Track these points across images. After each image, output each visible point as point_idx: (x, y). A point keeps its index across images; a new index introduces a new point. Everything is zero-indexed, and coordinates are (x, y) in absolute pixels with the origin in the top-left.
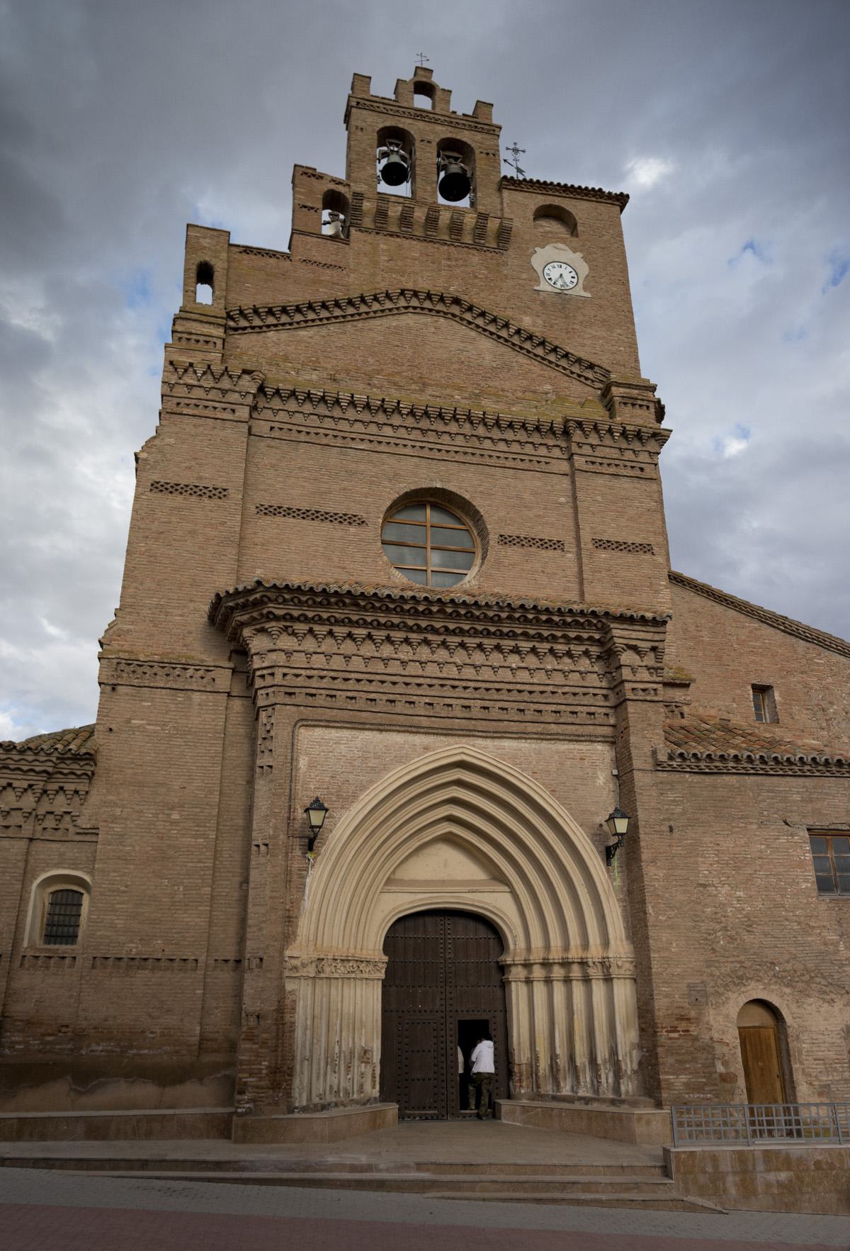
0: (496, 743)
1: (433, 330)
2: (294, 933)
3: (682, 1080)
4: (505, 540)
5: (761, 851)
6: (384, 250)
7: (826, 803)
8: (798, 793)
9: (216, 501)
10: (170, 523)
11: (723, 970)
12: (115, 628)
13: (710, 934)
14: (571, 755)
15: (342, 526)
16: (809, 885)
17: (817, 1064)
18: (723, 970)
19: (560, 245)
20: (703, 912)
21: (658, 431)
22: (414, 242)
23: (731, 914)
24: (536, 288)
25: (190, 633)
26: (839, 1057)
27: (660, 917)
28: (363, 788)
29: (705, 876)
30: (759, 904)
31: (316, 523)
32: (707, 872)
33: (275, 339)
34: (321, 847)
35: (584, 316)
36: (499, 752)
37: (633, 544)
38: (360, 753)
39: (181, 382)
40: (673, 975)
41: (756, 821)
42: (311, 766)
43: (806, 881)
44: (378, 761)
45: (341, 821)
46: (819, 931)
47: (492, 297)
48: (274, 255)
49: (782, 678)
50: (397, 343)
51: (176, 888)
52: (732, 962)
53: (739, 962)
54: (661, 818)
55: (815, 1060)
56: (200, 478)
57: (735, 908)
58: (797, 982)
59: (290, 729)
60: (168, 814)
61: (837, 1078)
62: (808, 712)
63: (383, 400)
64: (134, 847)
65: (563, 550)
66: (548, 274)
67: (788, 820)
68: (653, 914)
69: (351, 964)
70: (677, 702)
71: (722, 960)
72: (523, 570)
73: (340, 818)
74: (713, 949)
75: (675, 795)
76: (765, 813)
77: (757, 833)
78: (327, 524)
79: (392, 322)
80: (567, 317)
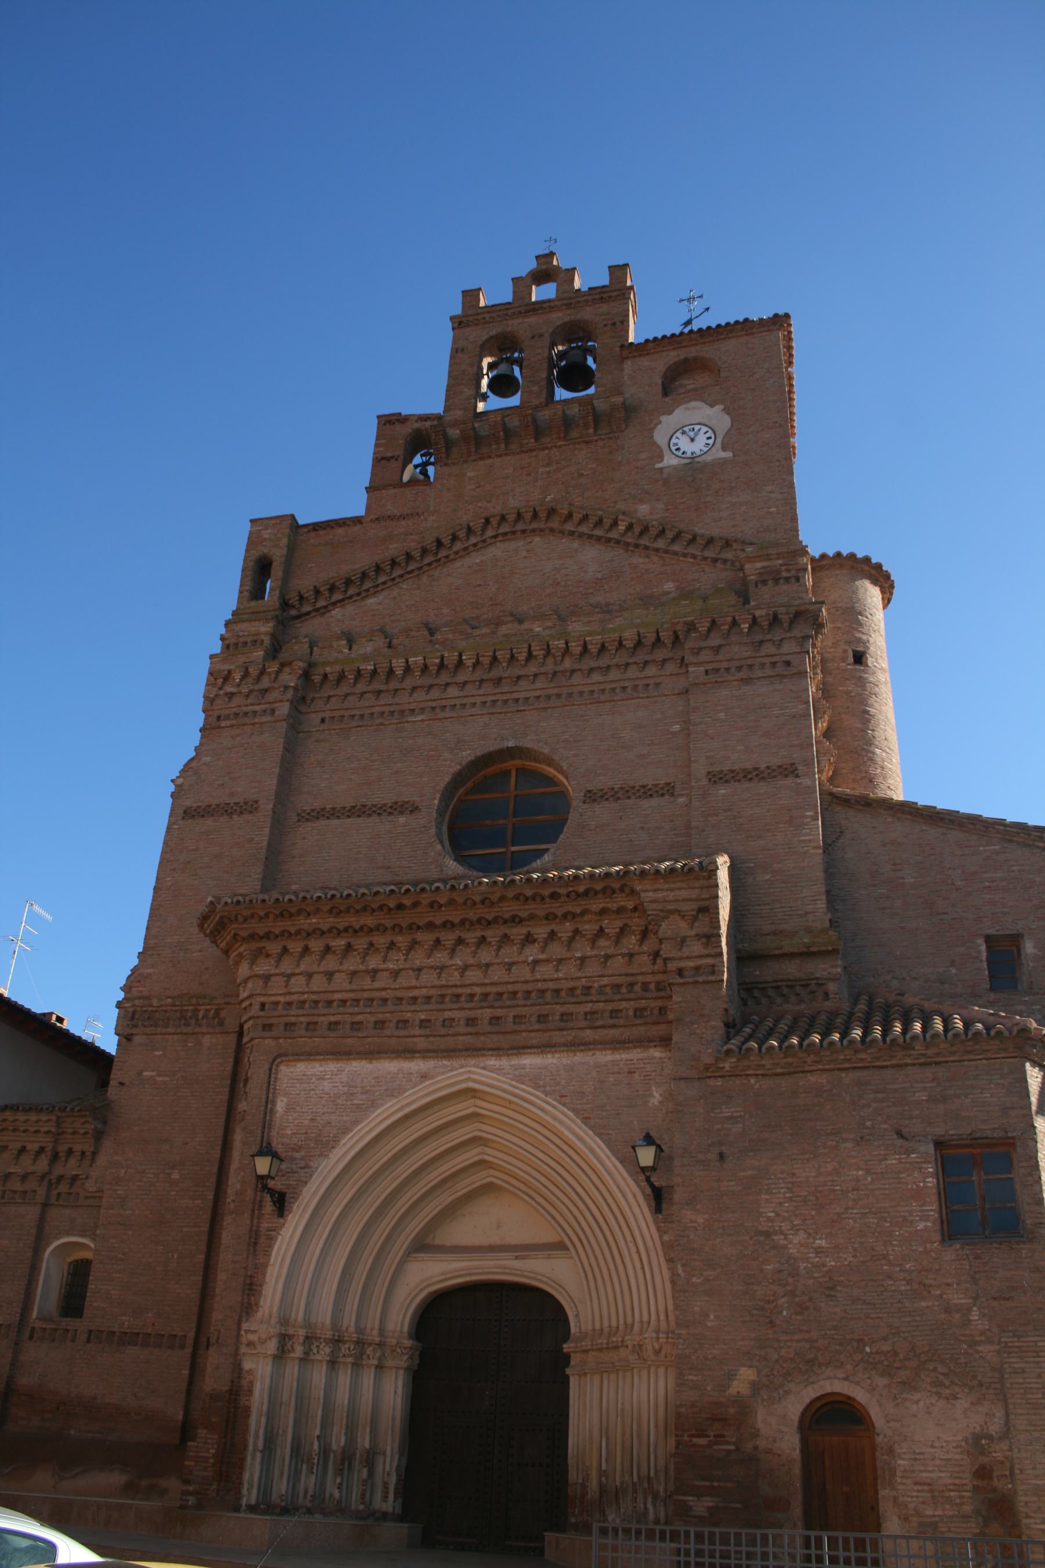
0: (513, 1062)
1: (524, 554)
2: (257, 1305)
3: (706, 1504)
4: (592, 797)
5: (857, 1180)
7: (968, 1100)
8: (924, 1089)
10: (197, 850)
11: (783, 1352)
12: (136, 974)
13: (769, 1302)
15: (391, 818)
16: (929, 1224)
17: (919, 1491)
18: (783, 1352)
19: (694, 404)
20: (762, 1271)
21: (802, 608)
22: (509, 458)
23: (804, 1272)
24: (658, 466)
25: (207, 969)
26: (957, 1481)
27: (694, 1280)
28: (346, 1130)
32: (772, 1215)
34: (294, 1203)
36: (517, 1073)
37: (768, 768)
38: (346, 1088)
39: (221, 692)
40: (706, 1359)
41: (852, 1136)
42: (289, 1108)
43: (924, 1218)
44: (364, 1097)
45: (318, 1171)
46: (938, 1292)
48: (344, 523)
50: (478, 583)
51: (170, 1255)
52: (799, 1341)
54: (710, 1141)
55: (916, 1484)
56: (232, 794)
57: (812, 1263)
58: (898, 1368)
59: (267, 1067)
61: (951, 1513)
63: (442, 657)
65: (672, 795)
67: (904, 1131)
68: (683, 1275)
69: (347, 1346)
70: (817, 978)
71: (783, 1338)
73: (317, 1168)
74: (771, 1322)
75: (732, 1110)
76: (868, 1124)
77: (854, 1154)
78: (375, 818)
79: (476, 558)
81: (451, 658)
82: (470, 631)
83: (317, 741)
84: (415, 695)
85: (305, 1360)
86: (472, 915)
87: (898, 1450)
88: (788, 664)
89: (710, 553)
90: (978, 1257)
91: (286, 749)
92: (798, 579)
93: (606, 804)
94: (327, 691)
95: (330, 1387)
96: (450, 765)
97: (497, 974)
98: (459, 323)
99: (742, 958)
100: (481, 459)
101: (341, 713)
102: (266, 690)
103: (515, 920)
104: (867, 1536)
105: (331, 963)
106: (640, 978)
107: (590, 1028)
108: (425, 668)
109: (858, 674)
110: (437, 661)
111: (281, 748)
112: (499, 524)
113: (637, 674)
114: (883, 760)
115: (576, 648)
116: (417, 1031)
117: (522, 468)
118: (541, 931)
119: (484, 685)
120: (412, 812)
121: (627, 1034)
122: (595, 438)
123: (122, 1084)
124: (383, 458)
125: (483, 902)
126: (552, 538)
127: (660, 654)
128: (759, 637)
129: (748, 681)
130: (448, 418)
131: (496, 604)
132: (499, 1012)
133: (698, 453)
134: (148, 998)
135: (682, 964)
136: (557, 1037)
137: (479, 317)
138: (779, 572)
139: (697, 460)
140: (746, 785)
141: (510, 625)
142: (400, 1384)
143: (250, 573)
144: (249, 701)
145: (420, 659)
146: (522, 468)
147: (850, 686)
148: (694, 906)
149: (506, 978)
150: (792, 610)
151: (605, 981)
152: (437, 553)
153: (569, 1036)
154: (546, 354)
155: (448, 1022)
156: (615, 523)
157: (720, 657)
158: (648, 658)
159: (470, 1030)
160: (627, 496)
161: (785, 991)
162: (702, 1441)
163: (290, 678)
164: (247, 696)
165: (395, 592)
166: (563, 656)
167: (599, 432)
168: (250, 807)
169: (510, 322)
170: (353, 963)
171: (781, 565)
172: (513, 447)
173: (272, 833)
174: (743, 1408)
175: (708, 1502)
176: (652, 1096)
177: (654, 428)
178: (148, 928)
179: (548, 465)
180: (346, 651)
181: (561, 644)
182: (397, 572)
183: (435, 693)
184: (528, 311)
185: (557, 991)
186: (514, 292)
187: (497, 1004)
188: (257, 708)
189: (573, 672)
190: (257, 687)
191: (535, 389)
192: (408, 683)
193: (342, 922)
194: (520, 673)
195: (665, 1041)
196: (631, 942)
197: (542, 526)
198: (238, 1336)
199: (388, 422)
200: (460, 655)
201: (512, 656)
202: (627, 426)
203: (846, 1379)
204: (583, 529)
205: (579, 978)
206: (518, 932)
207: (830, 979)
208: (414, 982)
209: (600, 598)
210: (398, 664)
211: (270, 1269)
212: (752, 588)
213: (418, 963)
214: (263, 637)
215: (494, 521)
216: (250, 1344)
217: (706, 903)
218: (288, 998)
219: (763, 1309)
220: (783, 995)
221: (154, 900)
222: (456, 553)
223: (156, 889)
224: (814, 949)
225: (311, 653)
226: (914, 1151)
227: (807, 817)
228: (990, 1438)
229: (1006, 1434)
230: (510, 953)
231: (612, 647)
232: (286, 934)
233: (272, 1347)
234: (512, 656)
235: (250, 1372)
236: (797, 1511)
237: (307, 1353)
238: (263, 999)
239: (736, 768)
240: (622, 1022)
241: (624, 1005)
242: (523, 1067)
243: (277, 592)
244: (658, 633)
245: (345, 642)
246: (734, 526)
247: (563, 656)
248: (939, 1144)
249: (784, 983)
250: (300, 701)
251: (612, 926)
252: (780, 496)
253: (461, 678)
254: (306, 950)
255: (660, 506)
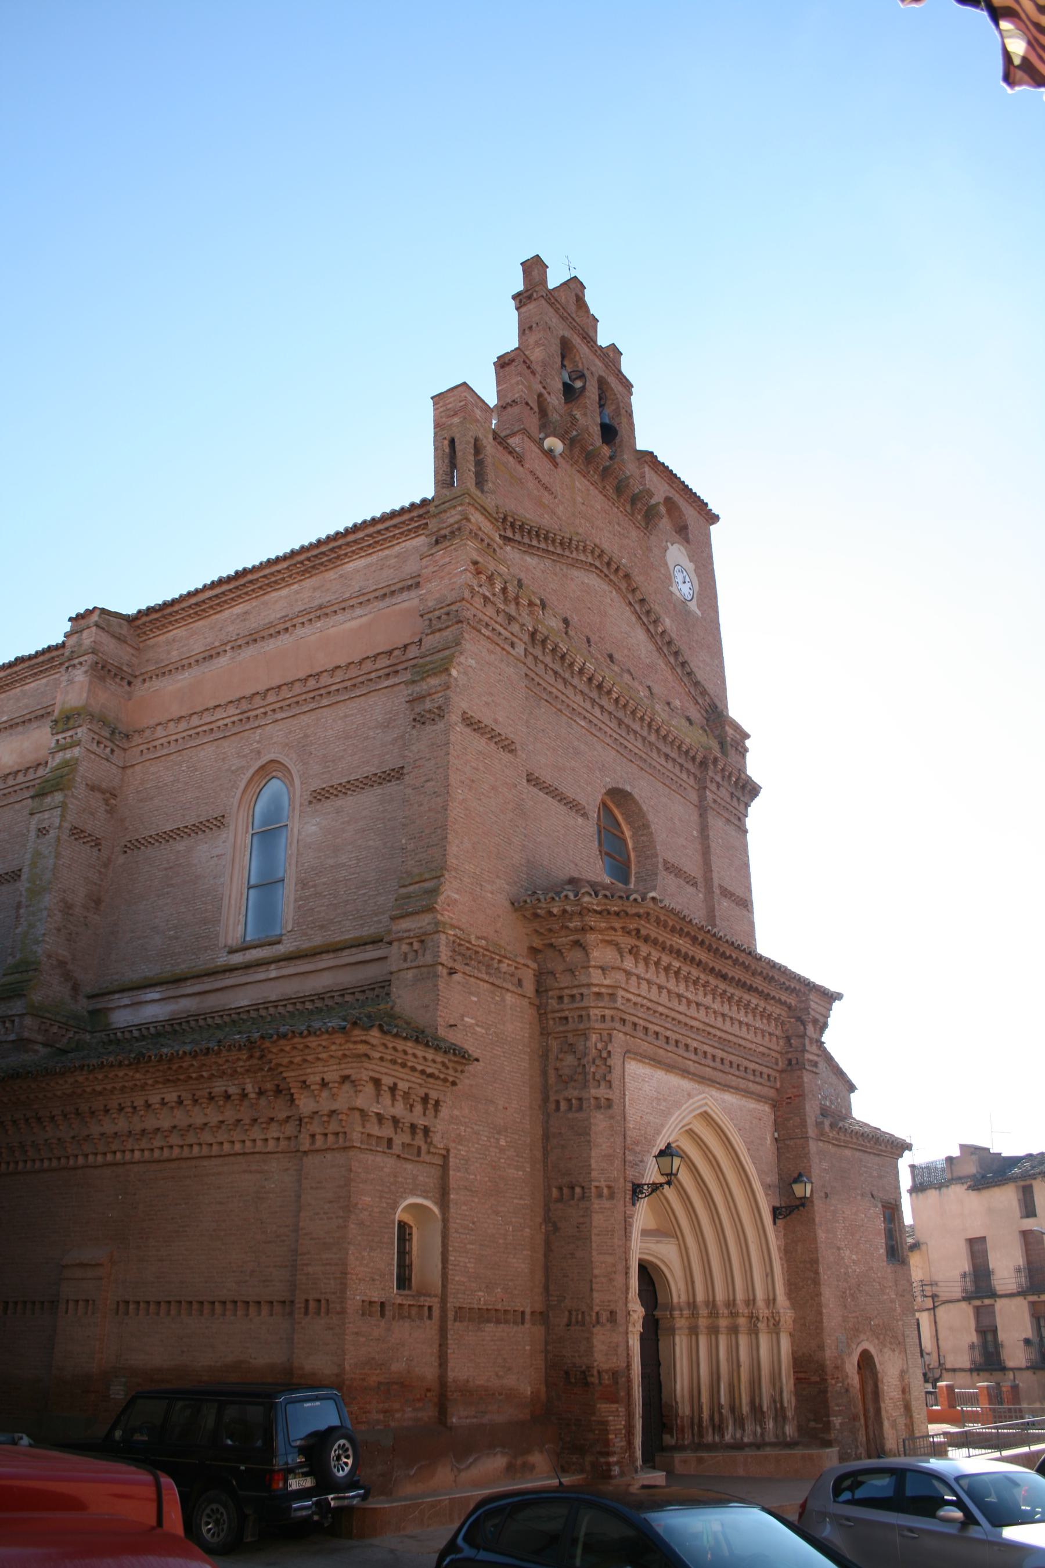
60: (497, 1139)
64: (476, 1176)
249: (234, 1011)
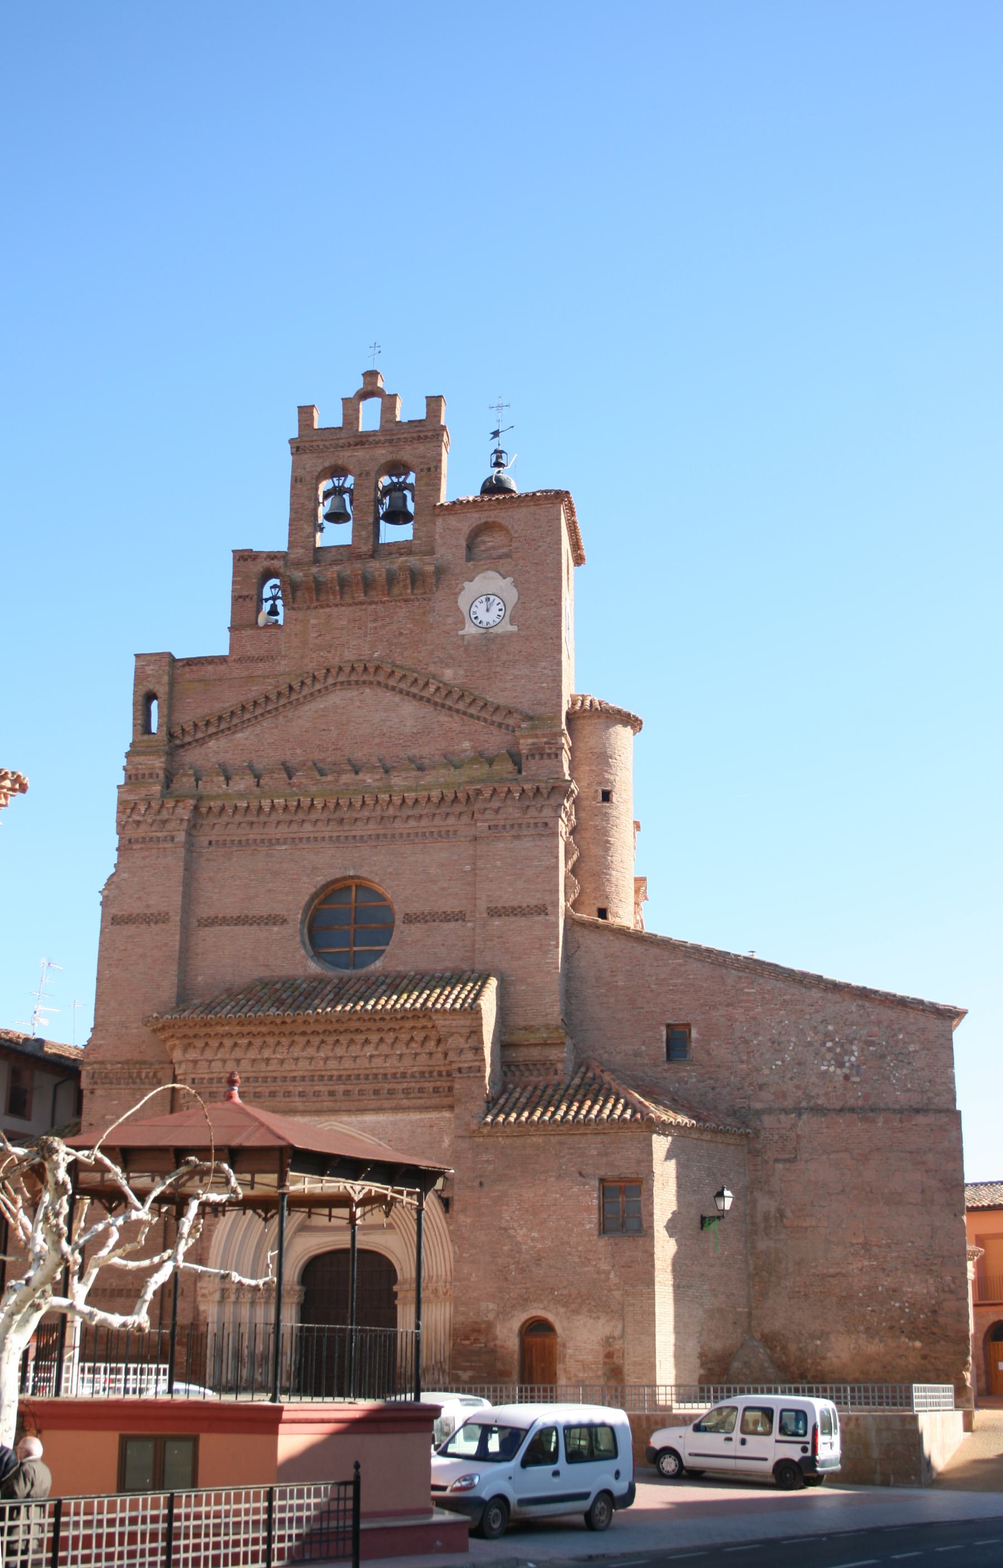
1: (358, 704)
4: (410, 919)
5: (556, 1200)
6: (314, 626)
8: (596, 1148)
9: (161, 925)
11: (512, 1295)
14: (422, 1124)
15: (267, 927)
18: (512, 1295)
22: (344, 608)
24: (461, 633)
25: (144, 1042)
29: (507, 1221)
30: (548, 1243)
31: (246, 927)
33: (215, 748)
35: (508, 654)
39: (130, 820)
43: (590, 1222)
47: (415, 655)
49: (703, 1013)
53: (526, 1288)
56: (148, 906)
62: (728, 1046)
63: (299, 801)
65: (464, 920)
66: (475, 613)
67: (584, 1172)
71: (512, 1287)
72: (424, 945)
78: (255, 927)
79: (320, 704)
80: (490, 660)
81: (306, 802)
82: (318, 777)
83: (207, 860)
84: (280, 827)
85: (236, 1302)
86: (330, 1028)
87: (568, 1344)
88: (546, 824)
89: (497, 718)
90: (616, 1244)
91: (186, 870)
92: (556, 755)
93: (418, 925)
94: (212, 820)
95: (252, 1316)
96: (309, 886)
97: (347, 1064)
98: (297, 448)
99: (504, 1044)
100: (322, 607)
101: (224, 838)
102: (166, 821)
103: (358, 1031)
104: (549, 1386)
105: (238, 1053)
106: (437, 1068)
107: (406, 1098)
108: (286, 808)
109: (604, 810)
110: (295, 803)
111: (182, 869)
112: (338, 674)
113: (441, 823)
114: (618, 879)
115: (397, 800)
116: (297, 1099)
117: (355, 621)
118: (375, 1038)
119: (331, 823)
120: (282, 924)
121: (429, 1102)
122: (412, 597)
123: (91, 1125)
124: (240, 597)
125: (337, 1021)
126: (379, 691)
127: (458, 808)
128: (527, 803)
129: (517, 837)
130: (292, 556)
131: (337, 749)
132: (349, 1087)
133: (492, 624)
134: (102, 1063)
135: (461, 1065)
136: (386, 1104)
137: (314, 444)
138: (543, 749)
139: (491, 630)
140: (513, 919)
141: (348, 776)
142: (294, 1312)
143: (140, 707)
144: (153, 829)
145: (282, 801)
146: (355, 621)
147: (597, 821)
148: (468, 1030)
149: (353, 1066)
150: (550, 786)
151: (415, 1069)
152: (289, 697)
153: (392, 1103)
154: (372, 497)
155: (317, 1094)
156: (427, 684)
157: (499, 816)
158: (449, 810)
159: (332, 1098)
160: (436, 660)
161: (531, 1067)
162: (467, 1342)
163: (184, 812)
164: (151, 825)
165: (258, 729)
166: (388, 805)
167: (416, 591)
168: (160, 918)
169: (342, 454)
170: (252, 1054)
171: (546, 743)
172: (348, 599)
173: (181, 938)
174: (490, 1325)
175: (469, 1373)
176: (443, 1141)
177: (459, 593)
178: (96, 1010)
179: (375, 620)
180: (224, 786)
181: (386, 797)
182: (259, 711)
183: (294, 827)
184: (356, 444)
185: (385, 1075)
186: (345, 415)
187: (348, 1082)
188: (159, 834)
189: (395, 817)
190: (158, 818)
191: (364, 533)
192: (274, 817)
193: (246, 1030)
194: (358, 816)
195: (451, 1107)
196: (431, 1044)
197: (371, 678)
198: (195, 1290)
199: (243, 558)
200: (312, 800)
201: (351, 803)
202: (437, 588)
203: (544, 1309)
204: (403, 685)
205: (398, 1067)
206: (360, 1038)
207: (558, 1061)
208: (294, 1067)
209: (414, 752)
210: (266, 804)
211: (211, 1250)
212: (524, 760)
213: (296, 1055)
214: (158, 771)
215: (334, 672)
216: (203, 1295)
217: (475, 1029)
218: (210, 1076)
219: (501, 1271)
220: (529, 1070)
221: (97, 988)
222: (305, 697)
223: (98, 980)
224: (549, 1042)
225: (197, 786)
226: (587, 1184)
227: (550, 945)
228: (614, 1338)
229: (622, 1336)
230: (355, 1050)
231: (423, 802)
232: (208, 1035)
233: (217, 1296)
234: (351, 803)
235: (204, 1311)
236: (515, 1376)
237: (237, 1298)
238: (193, 1076)
239: (507, 905)
240: (425, 1095)
241: (427, 1084)
242: (365, 1122)
243: (165, 728)
244: (456, 793)
245: (222, 778)
246: (515, 697)
247: (388, 805)
248: (602, 1180)
250: (193, 828)
251: (419, 1036)
252: (550, 673)
253: (314, 816)
254: (221, 1044)
255: (461, 672)
